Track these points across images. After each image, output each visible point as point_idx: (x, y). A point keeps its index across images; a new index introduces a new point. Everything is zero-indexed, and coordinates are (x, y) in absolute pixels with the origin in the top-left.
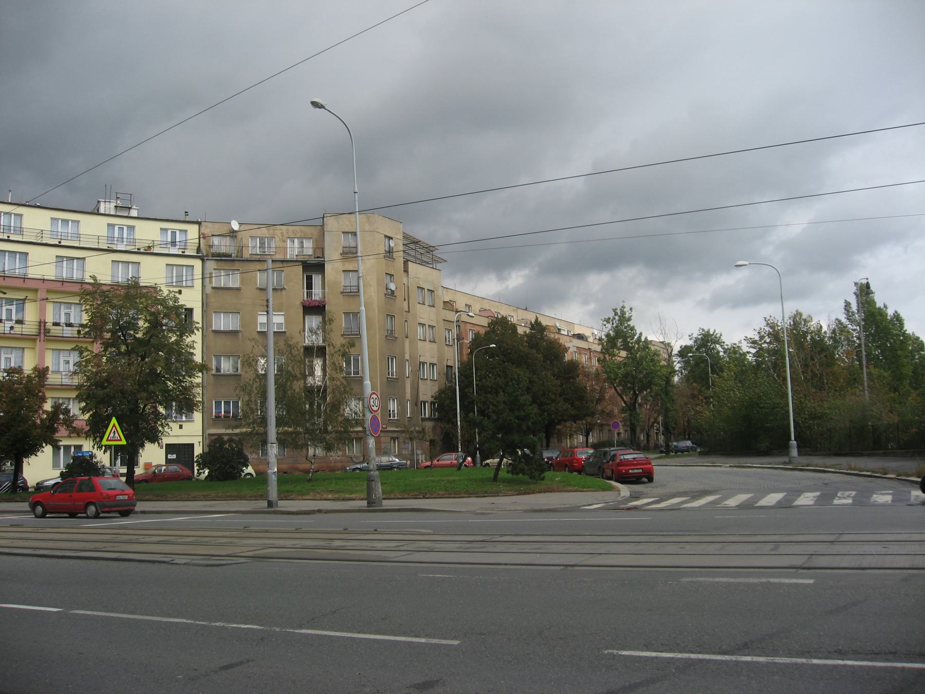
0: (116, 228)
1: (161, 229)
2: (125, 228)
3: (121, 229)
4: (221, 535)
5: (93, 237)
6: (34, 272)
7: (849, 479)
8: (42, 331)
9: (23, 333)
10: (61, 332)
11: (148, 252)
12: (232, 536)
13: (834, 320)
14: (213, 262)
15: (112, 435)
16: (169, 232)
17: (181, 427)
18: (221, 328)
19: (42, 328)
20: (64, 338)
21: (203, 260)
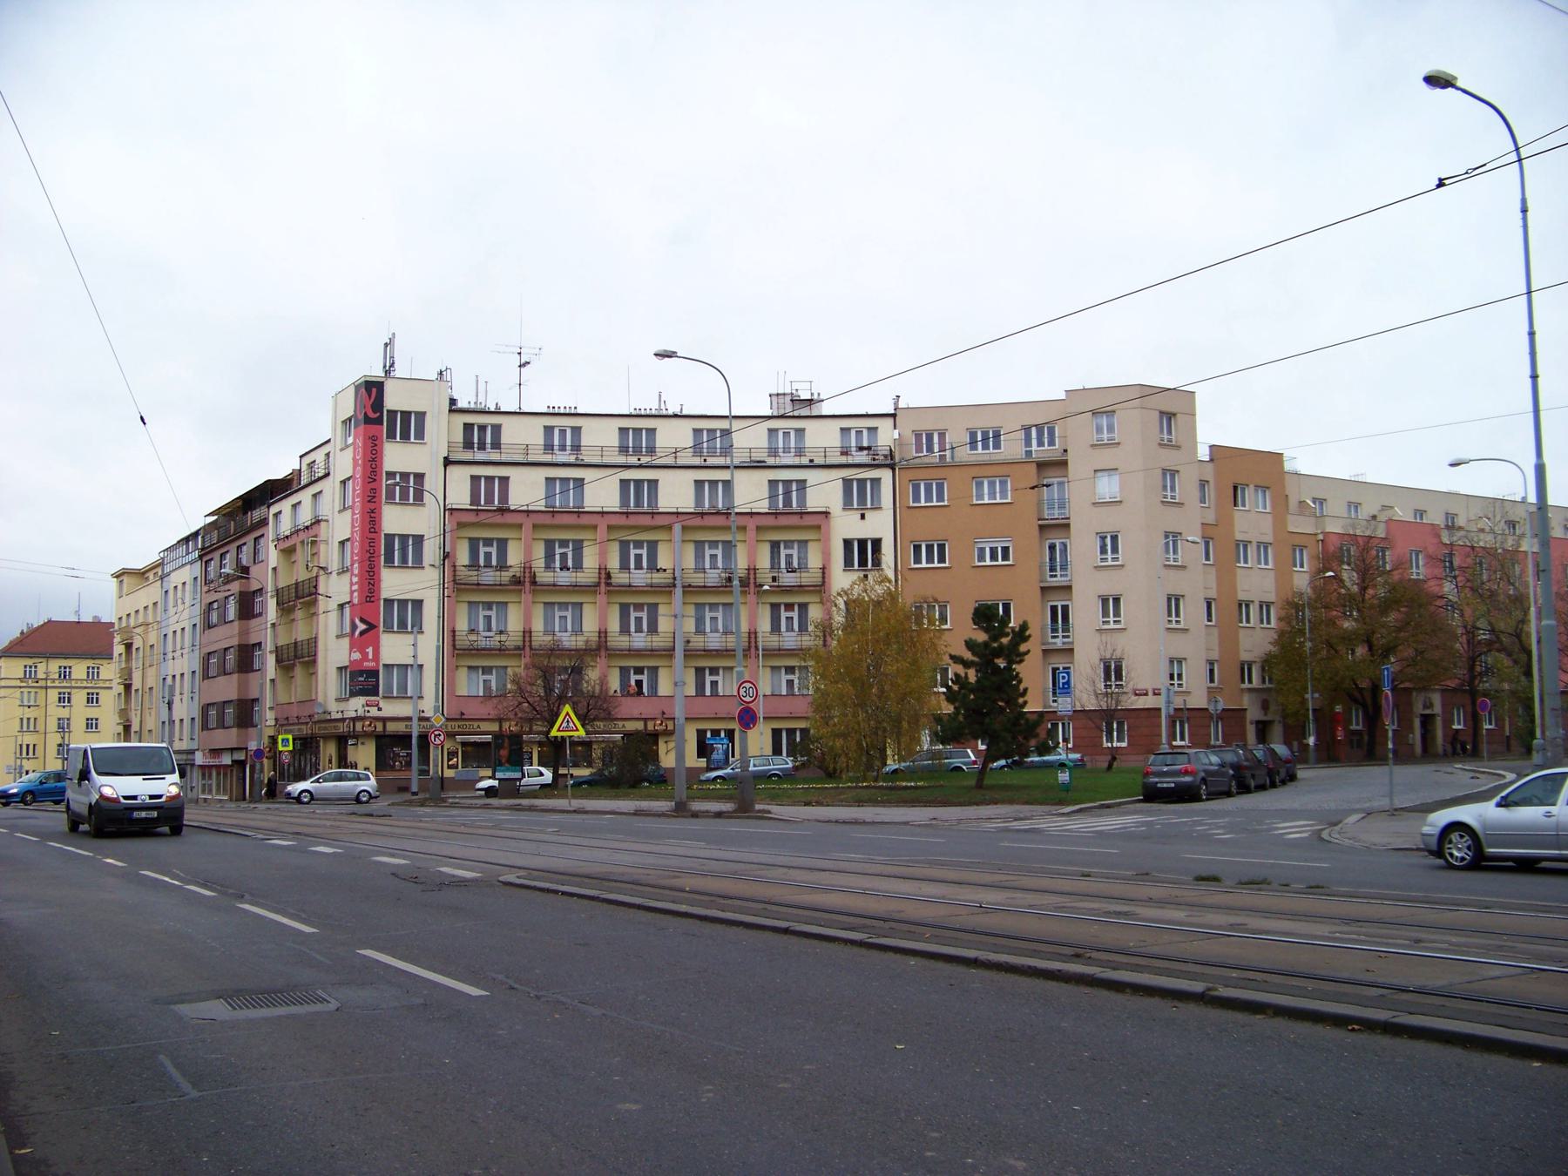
0: (853, 433)
1: (842, 429)
2: (865, 433)
3: (786, 434)
5: (611, 449)
6: (517, 499)
9: (706, 584)
10: (799, 580)
12: (1007, 884)
13: (1097, 661)
15: (565, 725)
16: (853, 433)
20: (557, 588)
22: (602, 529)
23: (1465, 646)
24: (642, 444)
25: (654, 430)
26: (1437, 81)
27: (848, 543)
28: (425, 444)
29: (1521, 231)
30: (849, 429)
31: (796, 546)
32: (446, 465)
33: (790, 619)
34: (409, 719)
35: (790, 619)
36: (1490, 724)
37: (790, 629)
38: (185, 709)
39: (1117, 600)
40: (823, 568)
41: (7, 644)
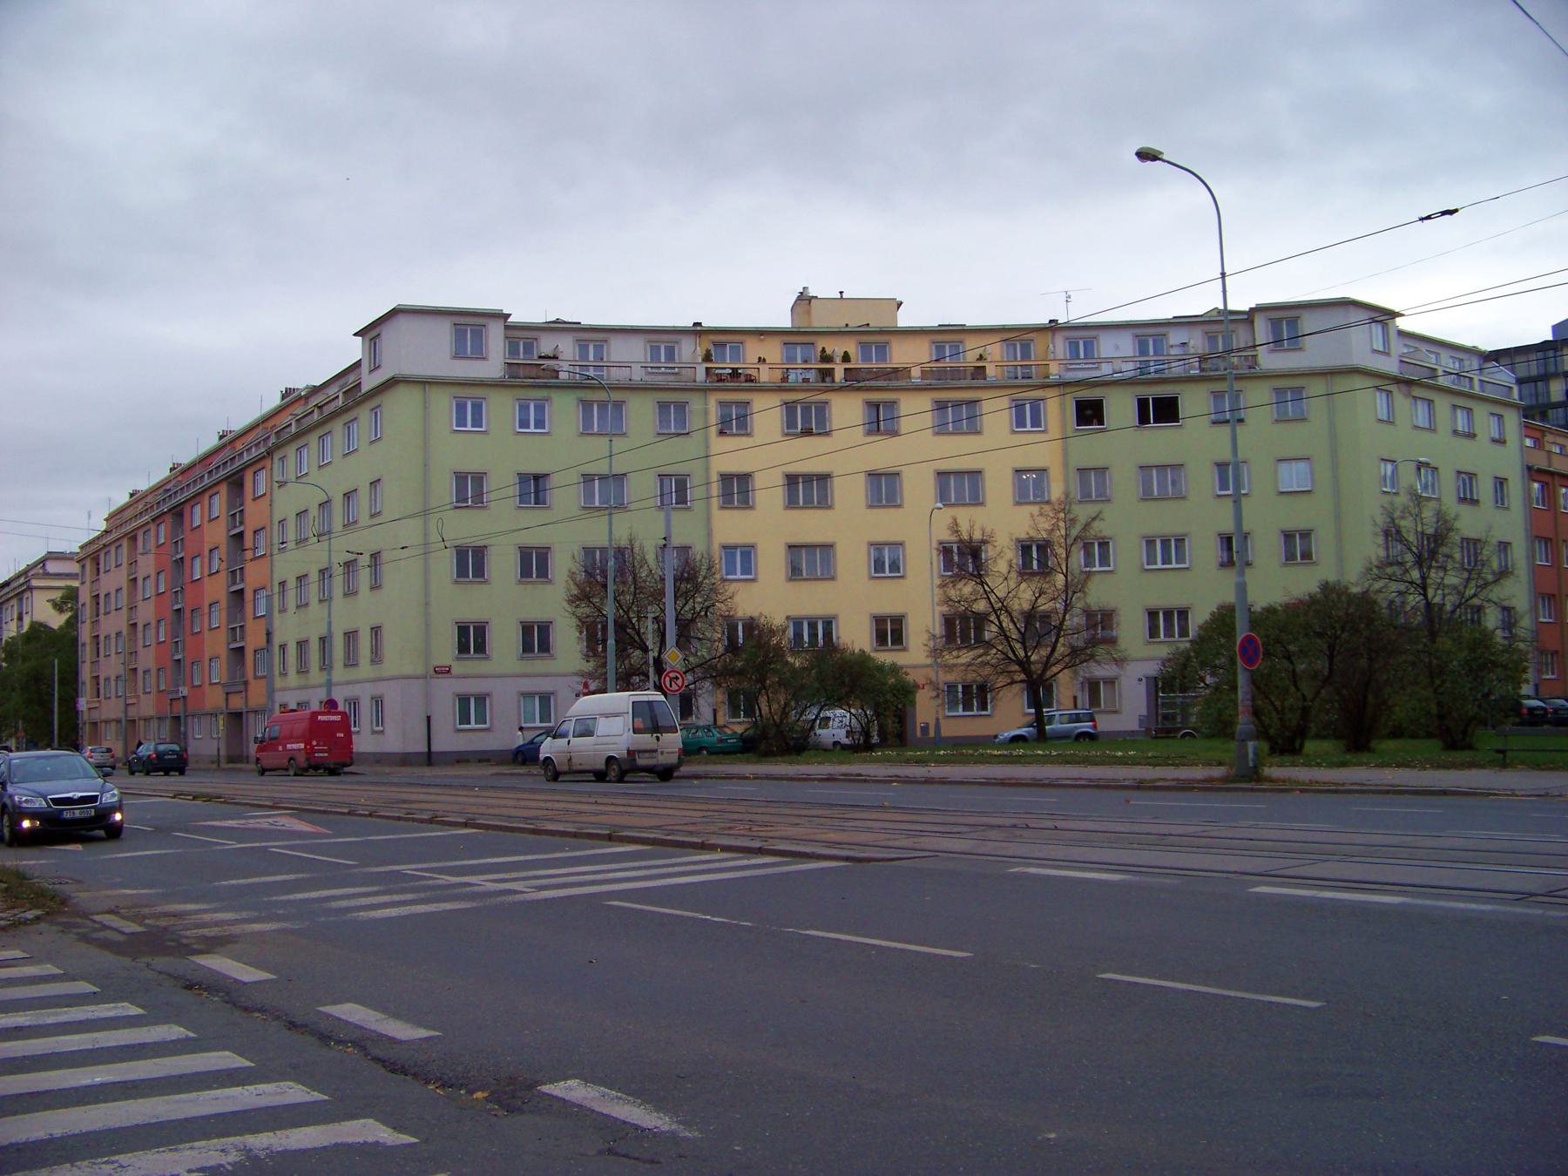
23: (1021, 625)
26: (1146, 155)
28: (376, 631)
36: (1553, 674)
39: (1180, 541)
41: (44, 554)
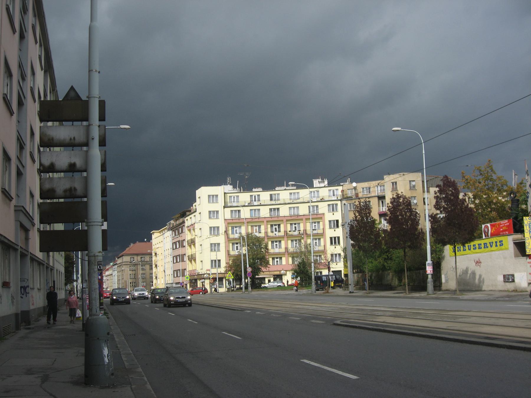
0: (232, 197)
3: (234, 197)
4: (482, 316)
6: (301, 213)
7: (68, 253)
8: (285, 234)
11: (322, 200)
14: (345, 201)
17: (337, 264)
18: (43, 226)
19: (285, 233)
21: (341, 201)
22: (304, 219)
24: (253, 199)
25: (259, 195)
27: (330, 221)
29: (515, 101)
30: (231, 196)
31: (317, 223)
32: (224, 208)
33: (276, 245)
34: (216, 274)
35: (276, 245)
37: (276, 247)
38: (170, 272)
40: (323, 229)
